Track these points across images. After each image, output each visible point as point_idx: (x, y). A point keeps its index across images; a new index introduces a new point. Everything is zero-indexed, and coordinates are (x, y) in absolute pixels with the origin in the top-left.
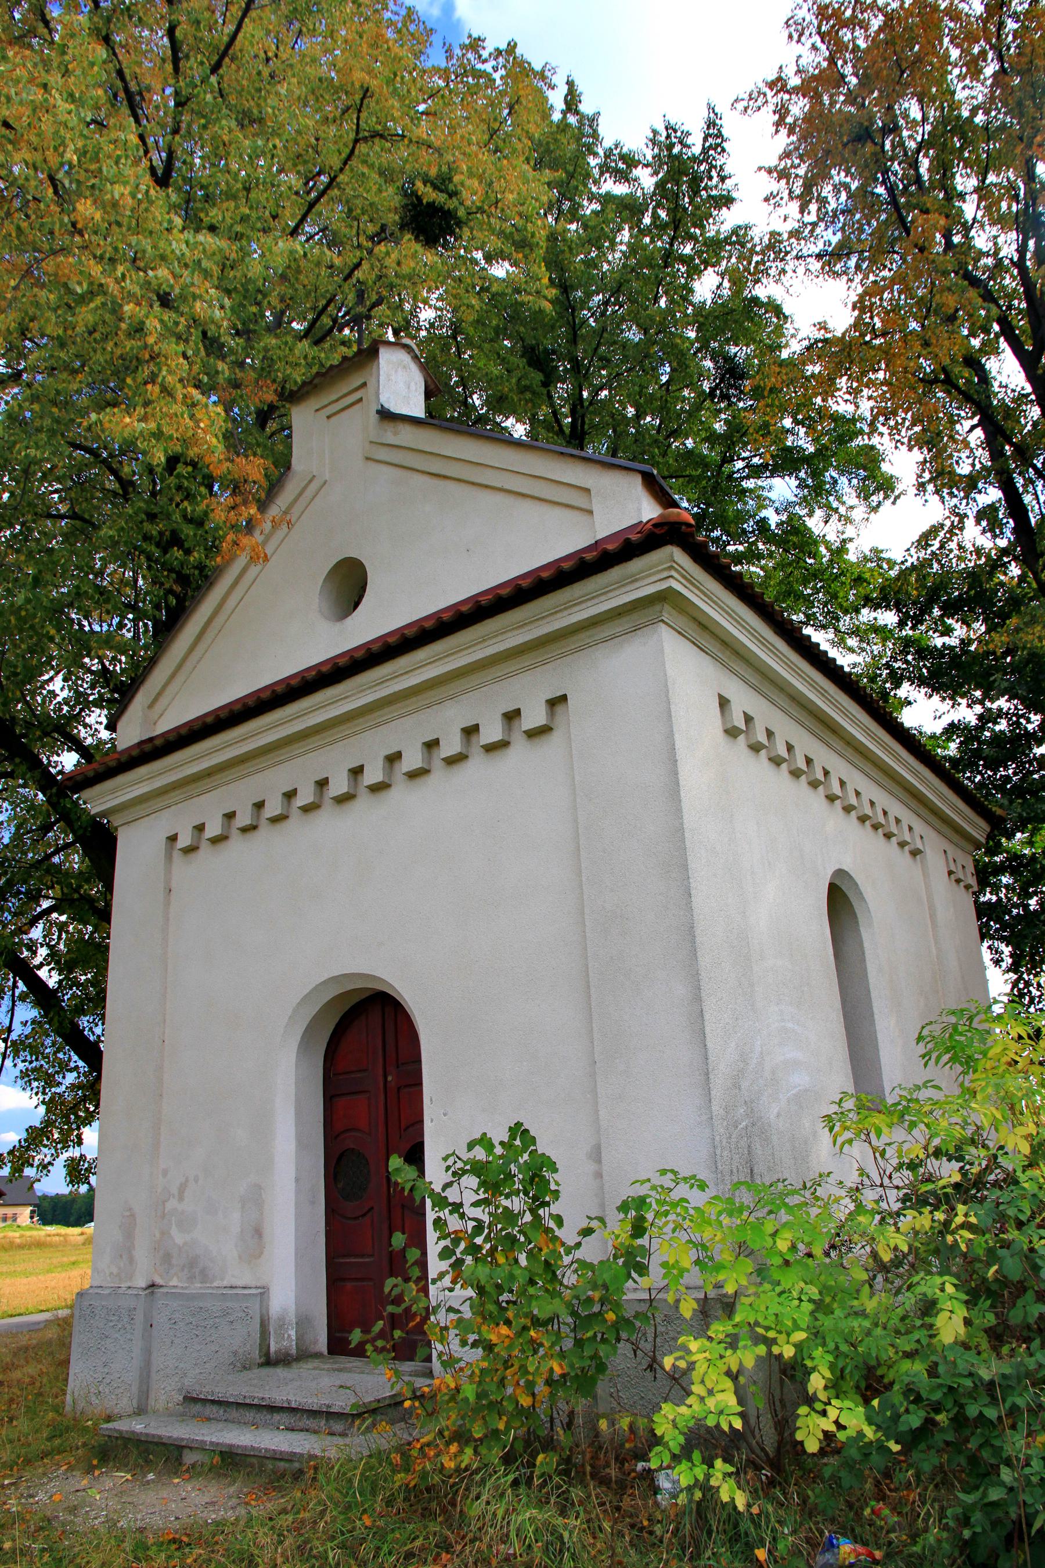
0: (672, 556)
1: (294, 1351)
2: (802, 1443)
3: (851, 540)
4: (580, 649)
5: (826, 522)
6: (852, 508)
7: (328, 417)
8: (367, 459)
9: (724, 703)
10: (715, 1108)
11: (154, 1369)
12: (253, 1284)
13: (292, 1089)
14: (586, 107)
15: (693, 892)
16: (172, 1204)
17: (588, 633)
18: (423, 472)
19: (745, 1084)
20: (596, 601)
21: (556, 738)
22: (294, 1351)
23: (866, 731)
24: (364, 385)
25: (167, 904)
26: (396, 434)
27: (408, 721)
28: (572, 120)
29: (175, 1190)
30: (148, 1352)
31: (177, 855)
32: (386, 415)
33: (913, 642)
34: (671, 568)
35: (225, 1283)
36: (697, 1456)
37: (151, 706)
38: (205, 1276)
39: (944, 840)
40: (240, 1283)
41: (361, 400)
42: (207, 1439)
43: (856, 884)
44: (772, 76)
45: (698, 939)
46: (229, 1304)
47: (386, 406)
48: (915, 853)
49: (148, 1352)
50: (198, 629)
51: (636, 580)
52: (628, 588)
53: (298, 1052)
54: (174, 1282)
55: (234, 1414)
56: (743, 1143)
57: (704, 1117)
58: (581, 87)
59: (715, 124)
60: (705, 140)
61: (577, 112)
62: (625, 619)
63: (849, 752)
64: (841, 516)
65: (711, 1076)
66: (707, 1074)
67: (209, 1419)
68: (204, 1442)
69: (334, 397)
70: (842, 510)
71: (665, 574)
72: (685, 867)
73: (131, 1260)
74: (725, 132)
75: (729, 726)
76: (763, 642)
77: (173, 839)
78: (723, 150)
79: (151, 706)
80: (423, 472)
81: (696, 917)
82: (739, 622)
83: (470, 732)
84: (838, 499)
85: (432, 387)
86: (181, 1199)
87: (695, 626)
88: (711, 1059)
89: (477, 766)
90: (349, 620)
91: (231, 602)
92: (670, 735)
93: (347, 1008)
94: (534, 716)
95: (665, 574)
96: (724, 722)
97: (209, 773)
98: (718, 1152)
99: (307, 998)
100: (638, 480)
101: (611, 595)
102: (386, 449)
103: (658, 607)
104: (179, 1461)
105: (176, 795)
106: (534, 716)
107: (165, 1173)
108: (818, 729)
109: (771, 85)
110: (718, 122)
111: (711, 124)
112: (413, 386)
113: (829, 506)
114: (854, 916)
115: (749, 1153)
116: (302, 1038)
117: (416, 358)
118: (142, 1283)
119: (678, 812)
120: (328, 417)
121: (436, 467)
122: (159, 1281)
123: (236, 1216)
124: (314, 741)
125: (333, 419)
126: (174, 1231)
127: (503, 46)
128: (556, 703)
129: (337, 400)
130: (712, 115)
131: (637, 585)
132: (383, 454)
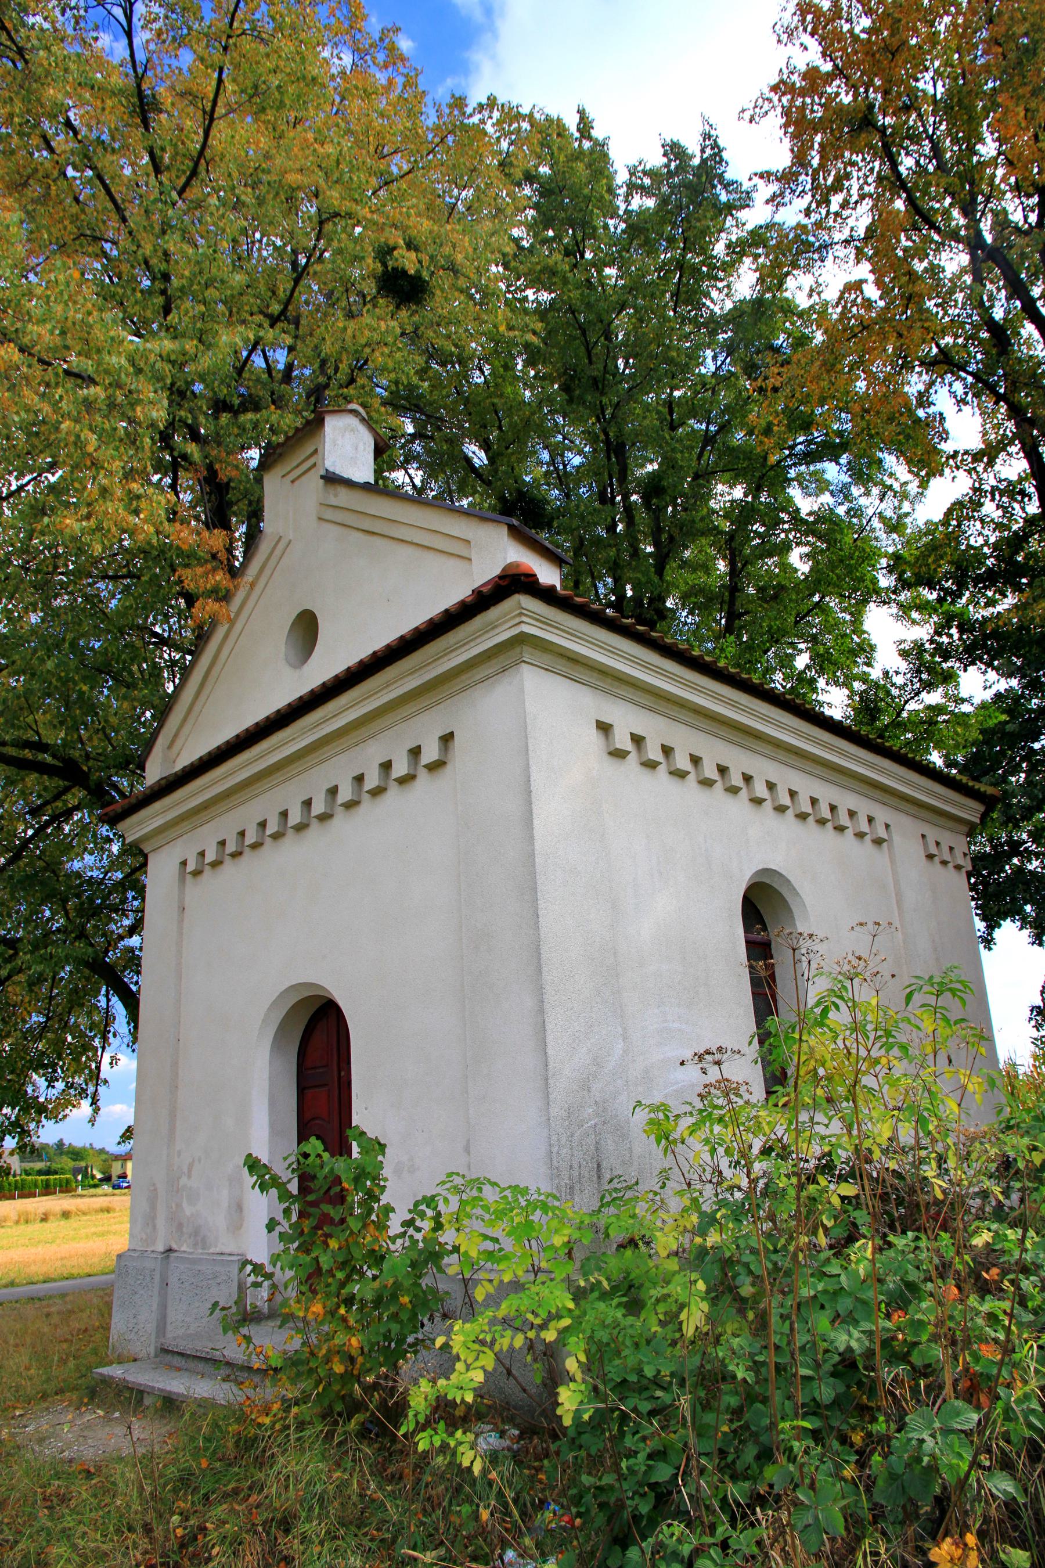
0: (519, 603)
1: (266, 1310)
2: (560, 1417)
3: (907, 515)
4: (463, 690)
5: (881, 500)
6: (906, 483)
7: (293, 482)
8: (320, 519)
9: (604, 728)
10: (554, 1111)
11: (169, 1321)
12: (236, 1251)
13: (266, 1084)
14: (597, 133)
15: (540, 913)
16: (184, 1180)
17: (469, 675)
18: (358, 529)
19: (596, 1087)
20: (467, 647)
21: (449, 768)
22: (266, 1310)
23: (796, 732)
24: (316, 451)
25: (181, 921)
26: (336, 496)
27: (343, 758)
28: (587, 145)
29: (185, 1170)
30: (163, 1307)
31: (189, 877)
32: (332, 479)
33: (956, 616)
34: (521, 614)
35: (218, 1250)
36: (442, 1425)
37: (170, 747)
38: (205, 1244)
39: (920, 823)
40: (227, 1250)
41: (314, 465)
42: (157, 1385)
43: (789, 881)
44: (774, 80)
45: (544, 956)
46: (217, 1268)
47: (331, 469)
48: (878, 842)
49: (163, 1307)
50: (202, 674)
51: (496, 627)
52: (491, 634)
53: (272, 1051)
54: (184, 1248)
55: (192, 1364)
56: (591, 1140)
57: (544, 1118)
58: (591, 113)
59: (710, 137)
60: (703, 151)
61: (590, 138)
62: (494, 661)
63: (781, 755)
64: (896, 492)
65: (551, 1081)
66: (547, 1079)
67: (179, 1369)
68: (153, 1388)
69: (295, 464)
70: (896, 486)
71: (517, 620)
72: (534, 889)
73: (154, 1227)
74: (721, 143)
75: (612, 749)
76: (646, 666)
77: (184, 863)
78: (722, 160)
79: (170, 747)
80: (358, 529)
81: (542, 935)
82: (613, 652)
83: (386, 766)
84: (891, 475)
85: (382, 444)
86: (189, 1177)
87: (564, 661)
88: (551, 1064)
89: (394, 794)
90: (306, 667)
91: (225, 652)
92: (527, 767)
93: (317, 1007)
94: (430, 753)
95: (517, 620)
96: (608, 746)
97: (205, 806)
98: (555, 1150)
99: (275, 1004)
100: (504, 530)
101: (478, 640)
102: (331, 510)
103: (518, 650)
104: (140, 1401)
105: (186, 825)
106: (430, 753)
107: (179, 1153)
108: (737, 737)
109: (774, 89)
110: (713, 133)
111: (707, 136)
112: (361, 447)
113: (882, 483)
114: (790, 911)
115: (597, 1149)
116: (275, 1038)
117: (363, 420)
118: (161, 1248)
119: (531, 839)
120: (293, 482)
121: (367, 524)
122: (175, 1246)
123: (225, 1192)
124: (279, 777)
125: (297, 483)
126: (185, 1204)
127: (484, 101)
128: (447, 739)
129: (297, 466)
130: (707, 127)
131: (497, 631)
132: (329, 514)
